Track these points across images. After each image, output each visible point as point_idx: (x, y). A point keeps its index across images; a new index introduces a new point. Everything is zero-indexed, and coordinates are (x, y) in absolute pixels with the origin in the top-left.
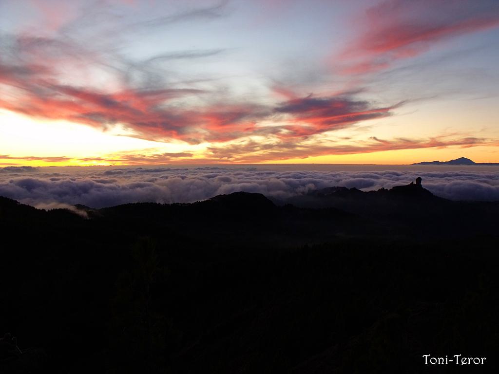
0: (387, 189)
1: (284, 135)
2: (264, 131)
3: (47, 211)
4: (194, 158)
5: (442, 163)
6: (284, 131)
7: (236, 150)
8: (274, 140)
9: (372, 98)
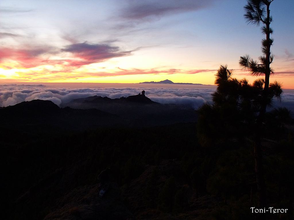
0: (125, 98)
1: (66, 66)
2: (53, 63)
5: (156, 83)
6: (66, 63)
7: (34, 74)
8: (59, 68)
9: (122, 45)
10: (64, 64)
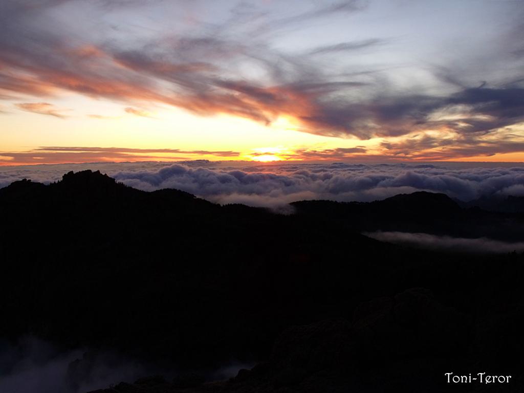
3: (222, 206)
4: (369, 153)
6: (436, 144)
7: (411, 145)
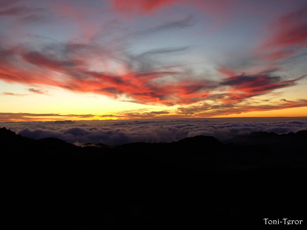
1: (226, 100)
5: (20, 122)
6: (226, 97)
7: (196, 109)
8: (220, 102)
9: (283, 74)
10: (225, 98)
